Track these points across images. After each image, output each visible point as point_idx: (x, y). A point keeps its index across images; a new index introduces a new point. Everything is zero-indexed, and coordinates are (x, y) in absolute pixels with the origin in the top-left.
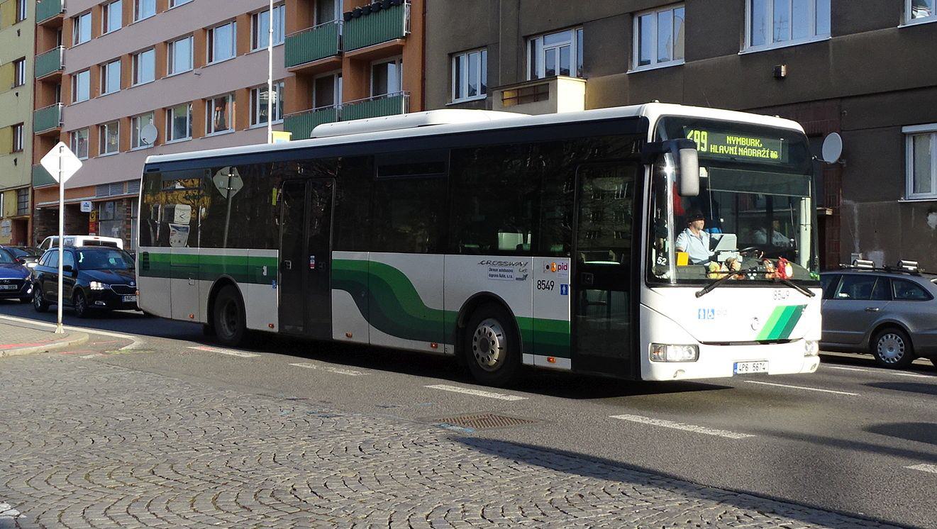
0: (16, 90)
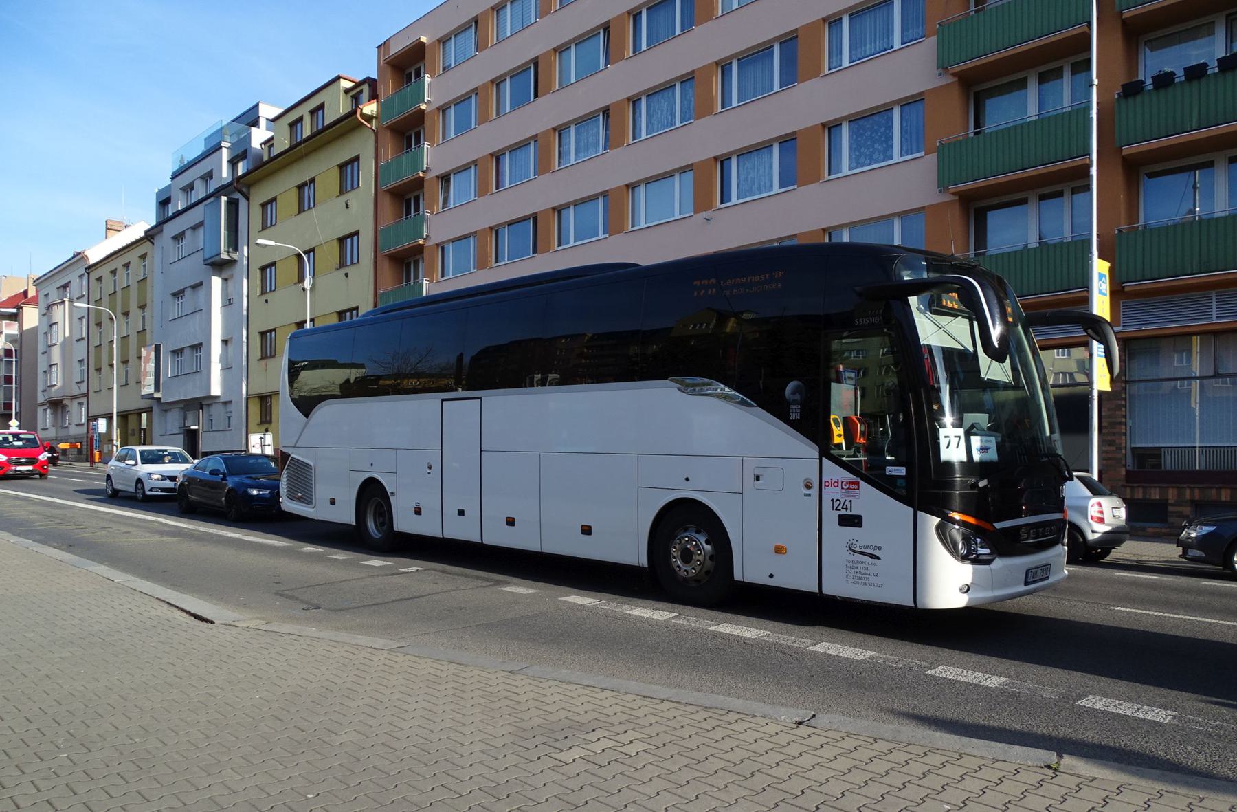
0: (346, 270)
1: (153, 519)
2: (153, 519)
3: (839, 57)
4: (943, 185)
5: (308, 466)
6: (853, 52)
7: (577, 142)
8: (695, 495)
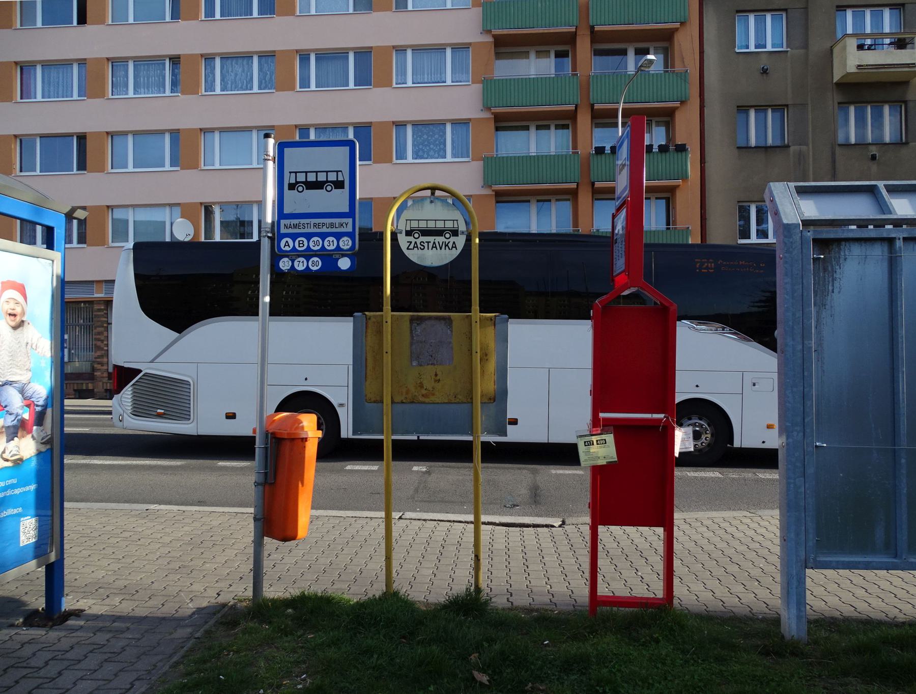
1: (570, 472)
2: (570, 472)
3: (403, 77)
4: (487, 184)
5: (188, 383)
6: (415, 77)
7: (136, 77)
8: (706, 396)
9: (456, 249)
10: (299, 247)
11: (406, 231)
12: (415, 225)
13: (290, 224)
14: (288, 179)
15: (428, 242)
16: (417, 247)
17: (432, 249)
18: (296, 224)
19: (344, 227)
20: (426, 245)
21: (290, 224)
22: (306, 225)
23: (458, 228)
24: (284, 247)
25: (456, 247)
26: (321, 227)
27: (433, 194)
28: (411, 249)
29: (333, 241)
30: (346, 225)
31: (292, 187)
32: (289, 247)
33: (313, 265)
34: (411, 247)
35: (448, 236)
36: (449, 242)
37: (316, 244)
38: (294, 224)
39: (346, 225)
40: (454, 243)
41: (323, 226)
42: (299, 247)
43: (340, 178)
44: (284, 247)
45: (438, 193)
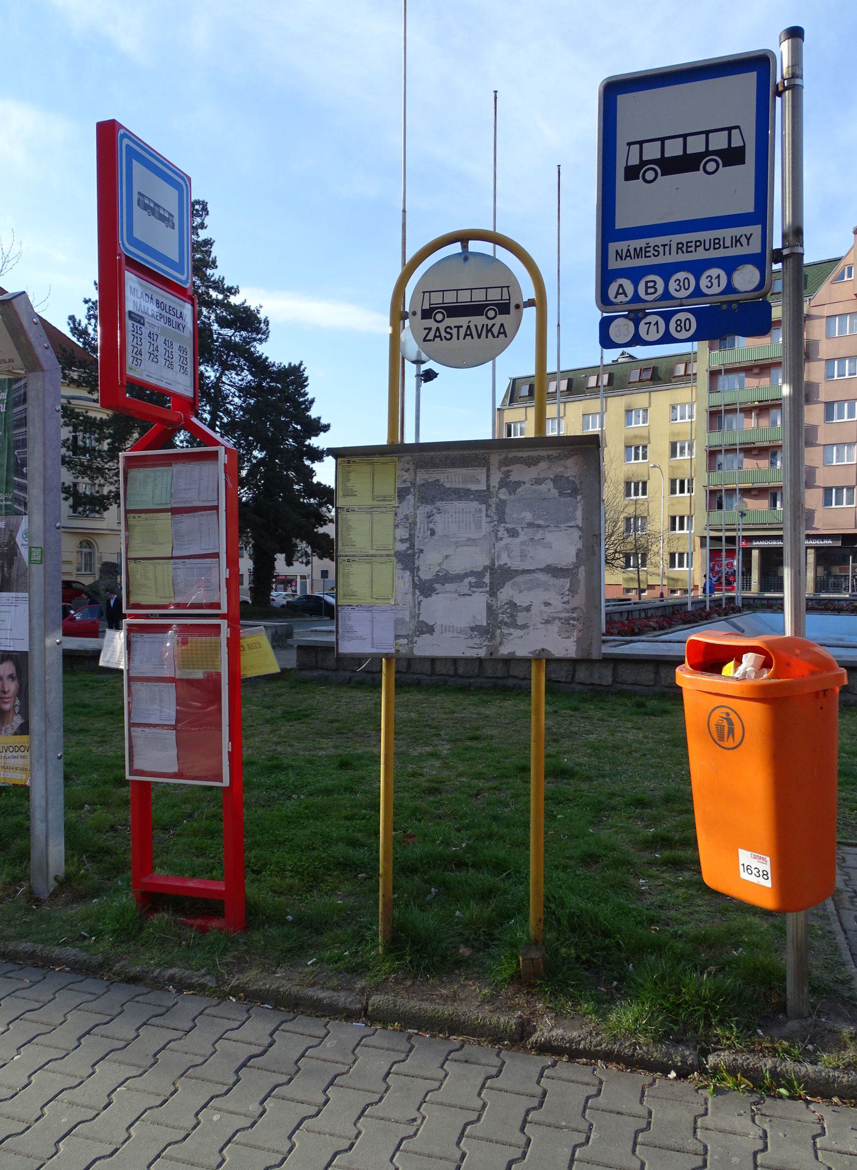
9: (506, 336)
10: (647, 294)
11: (423, 311)
12: (437, 299)
13: (628, 250)
14: (626, 157)
15: (458, 327)
16: (440, 336)
17: (464, 338)
18: (641, 249)
19: (742, 245)
20: (454, 332)
21: (628, 250)
22: (661, 249)
23: (509, 299)
24: (616, 297)
25: (504, 333)
26: (693, 249)
27: (465, 247)
28: (430, 340)
29: (718, 277)
30: (748, 239)
31: (632, 173)
32: (626, 296)
33: (679, 329)
34: (430, 336)
35: (491, 314)
36: (494, 325)
37: (681, 286)
38: (635, 249)
39: (748, 239)
40: (502, 325)
41: (696, 247)
42: (647, 294)
43: (736, 143)
44: (616, 297)
45: (474, 246)
